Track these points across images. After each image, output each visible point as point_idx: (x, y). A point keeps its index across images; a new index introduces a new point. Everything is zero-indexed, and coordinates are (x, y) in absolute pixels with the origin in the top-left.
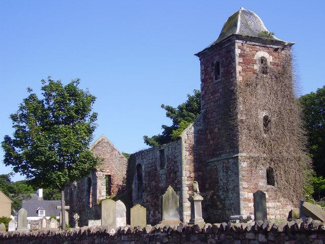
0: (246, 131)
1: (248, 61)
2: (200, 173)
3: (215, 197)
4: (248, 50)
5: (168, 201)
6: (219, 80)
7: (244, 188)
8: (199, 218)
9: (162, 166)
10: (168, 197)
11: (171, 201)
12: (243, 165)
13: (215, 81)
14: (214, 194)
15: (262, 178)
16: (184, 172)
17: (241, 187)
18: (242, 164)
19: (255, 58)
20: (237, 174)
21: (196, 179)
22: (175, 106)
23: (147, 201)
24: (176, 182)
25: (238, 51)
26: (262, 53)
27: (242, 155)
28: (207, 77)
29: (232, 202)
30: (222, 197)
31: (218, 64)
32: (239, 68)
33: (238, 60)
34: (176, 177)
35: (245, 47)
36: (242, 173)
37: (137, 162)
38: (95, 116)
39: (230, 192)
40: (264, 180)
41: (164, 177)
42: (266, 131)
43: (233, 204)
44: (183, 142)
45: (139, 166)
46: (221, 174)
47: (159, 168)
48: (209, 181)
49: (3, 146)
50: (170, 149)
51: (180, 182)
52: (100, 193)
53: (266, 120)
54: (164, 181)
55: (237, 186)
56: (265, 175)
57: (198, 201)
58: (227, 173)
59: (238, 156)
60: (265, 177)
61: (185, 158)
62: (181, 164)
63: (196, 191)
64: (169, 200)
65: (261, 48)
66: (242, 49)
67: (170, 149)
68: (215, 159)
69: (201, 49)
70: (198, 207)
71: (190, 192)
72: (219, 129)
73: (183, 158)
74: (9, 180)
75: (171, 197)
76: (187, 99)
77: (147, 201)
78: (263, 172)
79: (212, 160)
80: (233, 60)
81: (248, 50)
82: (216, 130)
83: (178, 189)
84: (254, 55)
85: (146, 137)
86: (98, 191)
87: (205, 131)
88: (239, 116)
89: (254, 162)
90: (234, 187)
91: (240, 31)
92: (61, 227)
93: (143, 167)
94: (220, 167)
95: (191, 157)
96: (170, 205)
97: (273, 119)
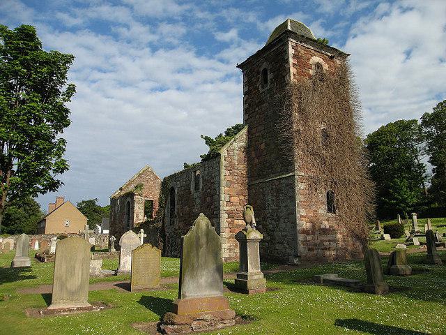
0: (302, 145)
1: (302, 64)
5: (197, 250)
7: (301, 216)
8: (255, 271)
9: (197, 188)
10: (198, 238)
11: (203, 250)
12: (301, 187)
15: (323, 203)
16: (223, 196)
17: (298, 215)
18: (300, 185)
19: (310, 62)
20: (293, 198)
21: (252, 201)
22: (213, 137)
23: (179, 228)
24: (212, 207)
25: (291, 51)
26: (316, 59)
27: (299, 174)
29: (284, 233)
31: (265, 71)
32: (293, 70)
33: (291, 61)
34: (212, 203)
35: (299, 49)
36: (299, 198)
38: (72, 90)
39: (282, 220)
40: (324, 206)
41: (198, 201)
43: (286, 236)
44: (223, 160)
45: (173, 189)
50: (207, 169)
51: (218, 208)
52: (137, 217)
53: (326, 134)
54: (199, 206)
55: (293, 213)
56: (325, 200)
57: (254, 240)
58: (277, 196)
59: (294, 175)
61: (225, 179)
62: (219, 186)
63: (251, 224)
64: (198, 246)
65: (316, 53)
66: (296, 50)
67: (207, 169)
70: (254, 254)
71: (230, 220)
72: (267, 145)
73: (222, 178)
74: (94, 204)
75: (203, 240)
77: (179, 228)
78: (322, 197)
80: (287, 61)
82: (263, 146)
83: (214, 216)
84: (308, 59)
86: (135, 215)
88: (294, 125)
89: (313, 183)
90: (288, 215)
93: (176, 191)
95: (241, 168)
96: (202, 260)
97: (333, 133)
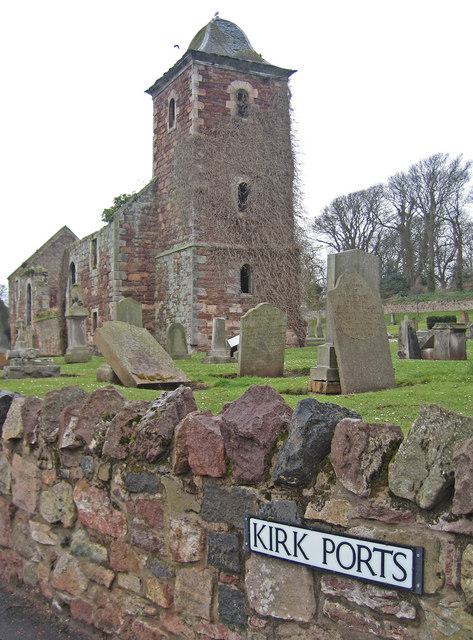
2: (146, 275)
3: (165, 312)
4: (215, 76)
6: (174, 127)
13: (169, 130)
14: (163, 308)
19: (228, 91)
28: (161, 124)
30: (172, 311)
37: (71, 260)
42: (242, 209)
45: (73, 265)
46: (172, 275)
47: (91, 269)
48: (157, 287)
49: (434, 160)
56: (238, 277)
60: (238, 281)
68: (166, 252)
69: (152, 83)
76: (292, 107)
78: (235, 273)
79: (163, 254)
81: (215, 76)
84: (225, 87)
85: (456, 177)
87: (156, 209)
91: (206, 48)
92: (195, 534)
94: (171, 264)
97: (255, 188)
